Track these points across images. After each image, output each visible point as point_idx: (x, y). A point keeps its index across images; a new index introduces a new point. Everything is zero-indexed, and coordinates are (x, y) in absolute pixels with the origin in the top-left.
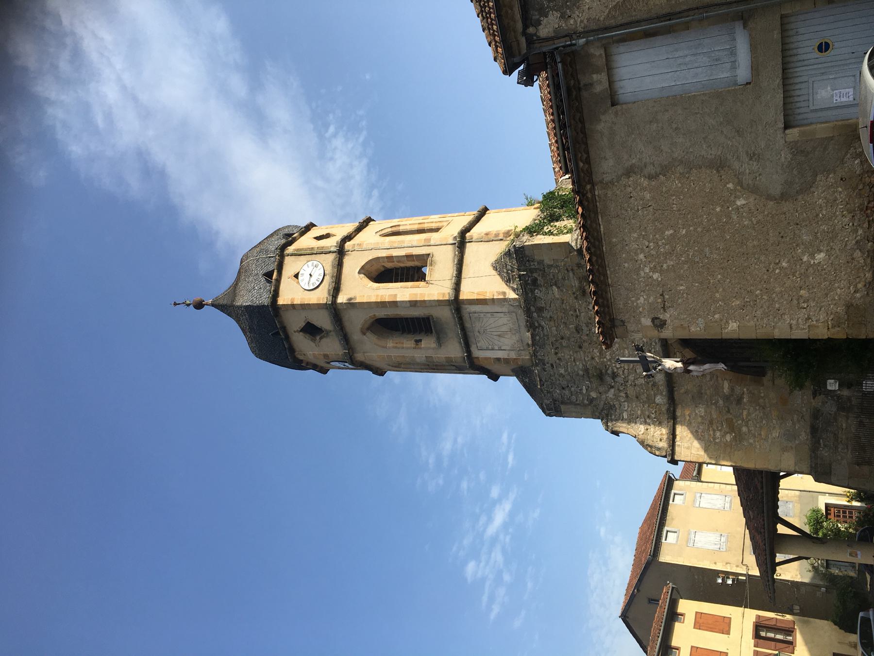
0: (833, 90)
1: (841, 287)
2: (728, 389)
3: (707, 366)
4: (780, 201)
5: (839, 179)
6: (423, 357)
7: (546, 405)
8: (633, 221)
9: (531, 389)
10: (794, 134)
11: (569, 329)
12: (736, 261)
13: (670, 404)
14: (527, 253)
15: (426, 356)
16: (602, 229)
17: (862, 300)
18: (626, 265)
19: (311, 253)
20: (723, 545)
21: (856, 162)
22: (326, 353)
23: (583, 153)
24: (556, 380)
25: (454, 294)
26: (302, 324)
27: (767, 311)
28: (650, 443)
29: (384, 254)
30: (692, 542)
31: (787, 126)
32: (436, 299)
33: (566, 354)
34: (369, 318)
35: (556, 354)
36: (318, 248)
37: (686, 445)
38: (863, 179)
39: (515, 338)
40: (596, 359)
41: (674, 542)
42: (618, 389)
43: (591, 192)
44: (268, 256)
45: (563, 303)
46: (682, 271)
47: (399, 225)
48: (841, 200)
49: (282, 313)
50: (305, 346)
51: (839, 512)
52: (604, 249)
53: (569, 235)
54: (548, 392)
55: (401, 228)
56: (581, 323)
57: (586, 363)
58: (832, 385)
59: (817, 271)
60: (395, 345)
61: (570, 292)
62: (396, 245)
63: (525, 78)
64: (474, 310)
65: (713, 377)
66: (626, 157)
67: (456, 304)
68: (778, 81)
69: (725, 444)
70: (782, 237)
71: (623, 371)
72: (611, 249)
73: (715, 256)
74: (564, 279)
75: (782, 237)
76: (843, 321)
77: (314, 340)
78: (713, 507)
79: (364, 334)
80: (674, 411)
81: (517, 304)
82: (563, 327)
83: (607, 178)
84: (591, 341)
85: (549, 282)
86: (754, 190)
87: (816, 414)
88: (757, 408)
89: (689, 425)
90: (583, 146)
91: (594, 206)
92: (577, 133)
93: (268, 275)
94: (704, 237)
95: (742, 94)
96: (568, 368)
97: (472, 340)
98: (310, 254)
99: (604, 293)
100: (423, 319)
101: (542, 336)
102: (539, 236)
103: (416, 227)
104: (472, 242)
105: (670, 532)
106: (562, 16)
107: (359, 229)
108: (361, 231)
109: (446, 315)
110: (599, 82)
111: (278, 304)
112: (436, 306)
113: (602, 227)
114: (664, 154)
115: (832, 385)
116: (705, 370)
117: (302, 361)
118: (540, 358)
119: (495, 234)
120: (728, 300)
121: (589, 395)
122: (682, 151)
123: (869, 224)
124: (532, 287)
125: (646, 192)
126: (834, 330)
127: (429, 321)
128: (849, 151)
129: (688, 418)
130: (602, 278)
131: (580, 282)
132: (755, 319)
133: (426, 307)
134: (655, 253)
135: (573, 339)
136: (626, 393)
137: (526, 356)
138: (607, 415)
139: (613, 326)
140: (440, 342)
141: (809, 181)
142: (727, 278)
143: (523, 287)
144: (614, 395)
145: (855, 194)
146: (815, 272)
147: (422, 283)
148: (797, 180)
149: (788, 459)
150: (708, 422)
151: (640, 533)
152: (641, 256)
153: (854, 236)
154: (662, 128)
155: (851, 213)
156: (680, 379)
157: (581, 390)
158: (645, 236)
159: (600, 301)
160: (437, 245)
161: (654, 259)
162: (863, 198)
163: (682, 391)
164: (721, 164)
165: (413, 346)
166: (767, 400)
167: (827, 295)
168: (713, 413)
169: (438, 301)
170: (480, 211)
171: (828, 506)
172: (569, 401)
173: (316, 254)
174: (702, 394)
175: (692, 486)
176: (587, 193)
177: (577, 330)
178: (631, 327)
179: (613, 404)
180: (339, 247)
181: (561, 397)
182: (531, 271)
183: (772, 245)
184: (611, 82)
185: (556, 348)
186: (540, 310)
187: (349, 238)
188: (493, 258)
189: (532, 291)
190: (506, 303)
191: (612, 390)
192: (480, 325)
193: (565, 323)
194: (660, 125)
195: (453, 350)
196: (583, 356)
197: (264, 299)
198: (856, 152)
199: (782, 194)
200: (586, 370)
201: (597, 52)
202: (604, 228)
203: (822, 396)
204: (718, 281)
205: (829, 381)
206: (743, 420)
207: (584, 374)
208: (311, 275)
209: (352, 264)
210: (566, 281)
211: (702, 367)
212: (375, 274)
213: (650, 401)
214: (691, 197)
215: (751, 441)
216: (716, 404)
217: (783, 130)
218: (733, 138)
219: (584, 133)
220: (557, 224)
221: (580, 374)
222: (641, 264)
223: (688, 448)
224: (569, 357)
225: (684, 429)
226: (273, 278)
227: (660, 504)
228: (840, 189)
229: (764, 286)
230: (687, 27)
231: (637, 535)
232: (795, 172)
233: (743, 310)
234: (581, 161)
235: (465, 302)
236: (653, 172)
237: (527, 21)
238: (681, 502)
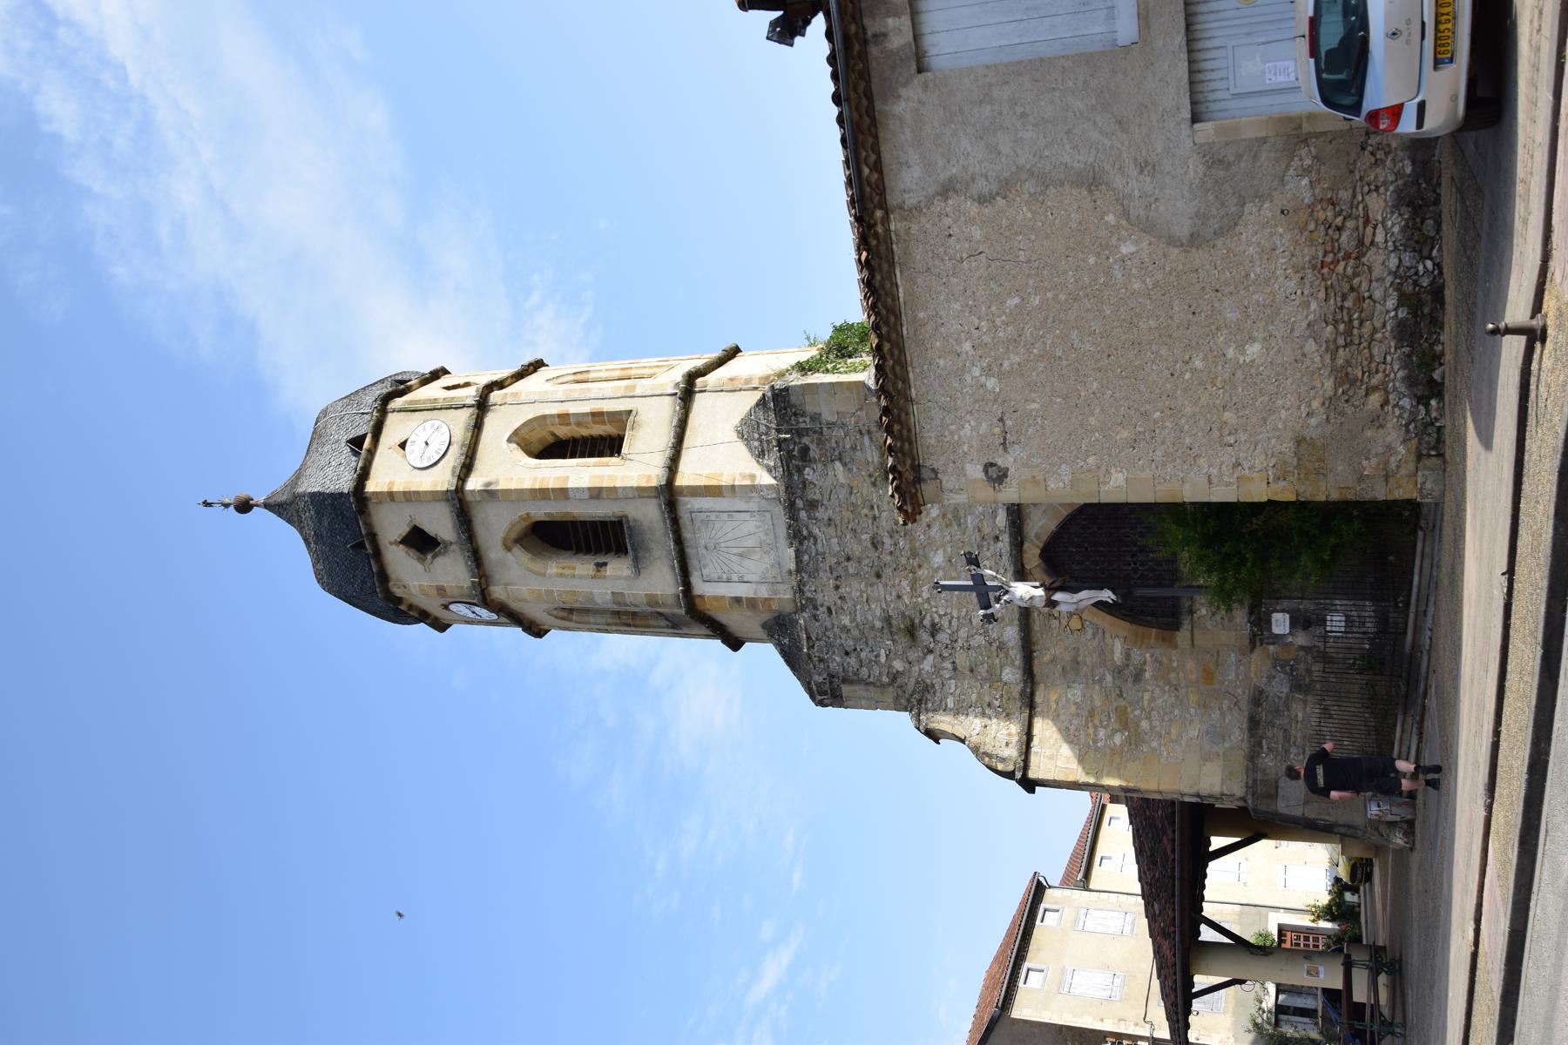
0: (1264, 62)
1: (1287, 407)
2: (1121, 654)
3: (1084, 594)
4: (1188, 248)
5: (1279, 211)
6: (607, 593)
7: (816, 685)
8: (954, 280)
9: (792, 658)
10: (1206, 130)
11: (860, 541)
12: (1122, 356)
13: (1025, 682)
14: (793, 399)
15: (613, 593)
16: (901, 295)
17: (1320, 429)
18: (942, 362)
19: (433, 408)
20: (1116, 992)
21: (1303, 183)
22: (441, 584)
23: (870, 152)
24: (835, 639)
25: (666, 475)
26: (404, 530)
27: (1171, 449)
28: (988, 748)
30: (1067, 986)
31: (1195, 118)
32: (635, 485)
33: (853, 589)
34: (518, 519)
35: (837, 588)
36: (444, 399)
37: (1048, 752)
38: (1315, 213)
39: (768, 560)
40: (905, 597)
41: (1039, 987)
42: (941, 655)
43: (883, 225)
44: (361, 411)
45: (851, 493)
46: (1034, 374)
48: (1282, 250)
49: (372, 508)
50: (410, 575)
51: (1298, 938)
52: (905, 332)
54: (821, 660)
56: (880, 532)
57: (888, 605)
58: (1280, 623)
59: (1249, 377)
60: (560, 571)
61: (863, 473)
62: (576, 396)
63: (778, 29)
64: (700, 506)
65: (1098, 632)
66: (941, 162)
68: (1180, 39)
69: (1112, 750)
70: (1194, 313)
71: (950, 622)
72: (915, 331)
73: (1088, 346)
74: (854, 448)
75: (1194, 313)
76: (1292, 469)
77: (422, 561)
78: (1106, 931)
79: (509, 549)
80: (1032, 694)
81: (774, 495)
82: (852, 538)
83: (911, 200)
84: (898, 565)
85: (829, 454)
86: (1147, 227)
87: (1258, 698)
88: (1167, 688)
89: (1056, 719)
90: (871, 140)
91: (887, 249)
92: (861, 116)
93: (357, 443)
94: (1070, 311)
95: (1125, 58)
96: (856, 616)
97: (693, 563)
98: (431, 410)
99: (903, 414)
100: (613, 523)
101: (813, 554)
102: (816, 375)
103: (617, 374)
104: (705, 391)
105: (1033, 970)
107: (520, 375)
108: (523, 378)
109: (650, 515)
110: (897, 31)
111: (366, 490)
112: (634, 498)
113: (901, 290)
114: (1003, 160)
115: (1280, 623)
116: (1081, 600)
117: (400, 600)
118: (809, 595)
119: (745, 379)
120: (1109, 429)
121: (890, 667)
122: (1032, 154)
123: (1327, 294)
124: (800, 464)
125: (974, 227)
126: (1277, 486)
127: (622, 524)
128: (1292, 163)
129: (1054, 706)
130: (900, 384)
132: (1153, 466)
133: (617, 499)
134: (990, 341)
135: (867, 561)
136: (954, 663)
137: (786, 594)
138: (920, 702)
139: (918, 480)
141: (1232, 213)
142: (1108, 388)
143: (784, 462)
145: (1304, 240)
146: (1245, 378)
148: (1214, 212)
150: (1087, 713)
152: (967, 346)
153: (1305, 313)
154: (1000, 113)
155: (1298, 272)
156: (1044, 636)
157: (876, 656)
158: (974, 309)
159: (896, 428)
160: (645, 396)
161: (988, 351)
162: (1316, 246)
163: (1047, 658)
164: (1094, 178)
165: (592, 573)
166: (1181, 673)
167: (1265, 420)
168: (1095, 698)
170: (726, 351)
171: (1282, 930)
172: (855, 678)
173: (441, 409)
174: (1078, 663)
175: (1073, 897)
176: (875, 224)
177: (873, 543)
178: (948, 481)
179: (932, 683)
180: (481, 397)
181: (844, 669)
182: (800, 433)
183: (1178, 327)
184: (917, 36)
185: (838, 578)
186: (812, 505)
187: (500, 385)
188: (736, 420)
189: (800, 471)
190: (754, 494)
191: (930, 657)
192: (709, 534)
193: (854, 531)
194: (996, 107)
195: (660, 582)
196: (882, 592)
197: (345, 483)
198: (1302, 165)
199: (1192, 235)
200: (888, 620)
202: (904, 293)
204: (1094, 393)
206: (1143, 709)
207: (883, 627)
208: (427, 444)
209: (499, 425)
210: (859, 453)
211: (1075, 595)
212: (537, 448)
213: (993, 677)
214: (1047, 237)
215: (1154, 744)
217: (1189, 124)
218: (1113, 134)
219: (871, 111)
221: (876, 627)
222: (966, 361)
223: (1051, 758)
224: (858, 594)
225: (1047, 724)
226: (363, 447)
227: (1020, 925)
228: (1281, 230)
229: (1167, 403)
232: (1211, 198)
233: (1134, 448)
234: (867, 165)
235: (685, 492)
236: (986, 191)
238: (1055, 922)
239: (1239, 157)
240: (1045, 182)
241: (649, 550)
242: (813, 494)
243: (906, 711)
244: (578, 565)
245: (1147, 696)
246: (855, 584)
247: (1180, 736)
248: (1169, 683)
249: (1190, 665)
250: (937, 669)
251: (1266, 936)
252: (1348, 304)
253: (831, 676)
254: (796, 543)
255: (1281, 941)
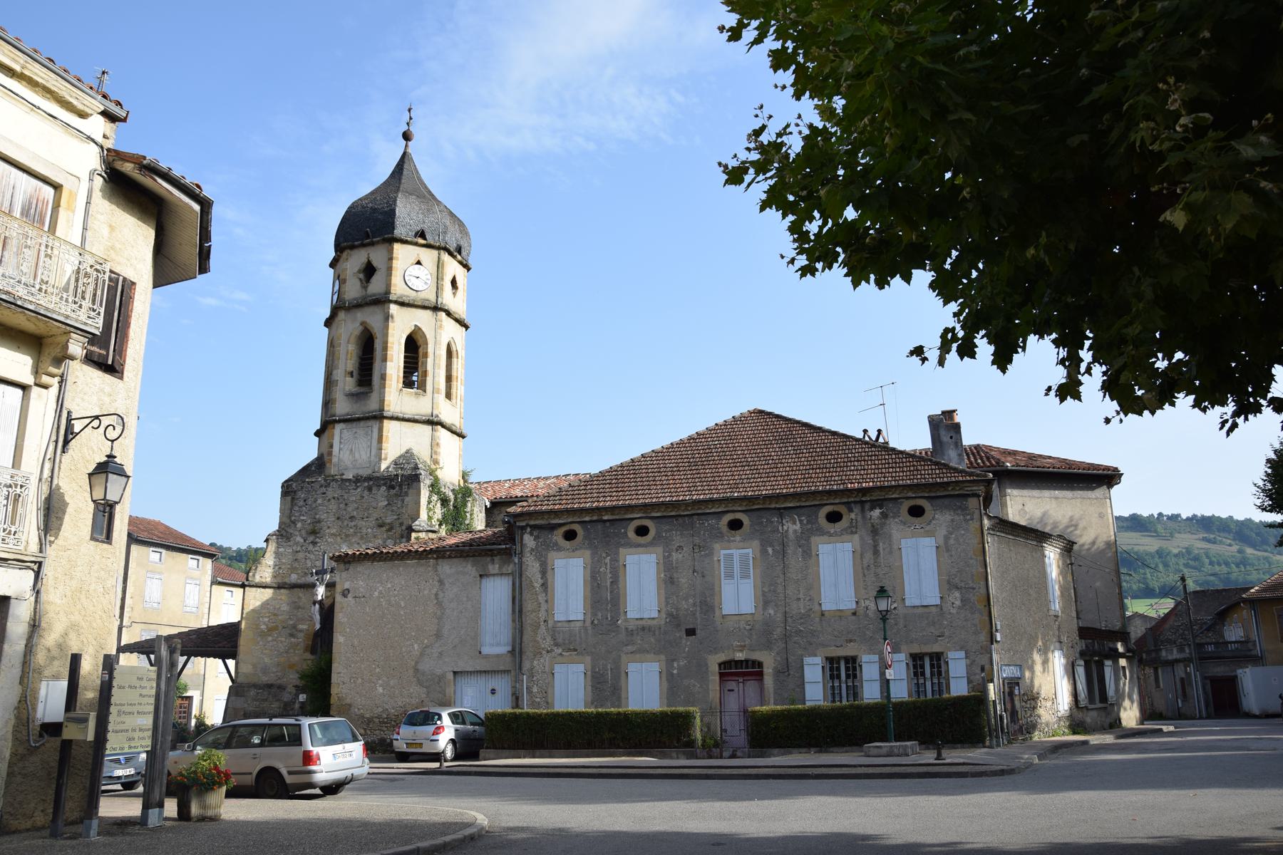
9: (305, 471)
10: (451, 676)
11: (353, 511)
19: (439, 278)
26: (375, 264)
29: (430, 350)
30: (152, 576)
31: (455, 673)
33: (333, 506)
35: (334, 498)
39: (348, 463)
47: (457, 358)
49: (387, 245)
50: (356, 260)
51: (185, 708)
53: (426, 517)
54: (302, 488)
55: (454, 360)
58: (302, 697)
67: (379, 417)
68: (478, 669)
77: (359, 272)
80: (284, 588)
83: (439, 568)
86: (422, 654)
87: (281, 688)
89: (272, 599)
97: (349, 425)
103: (454, 374)
106: (532, 550)
115: (302, 697)
121: (299, 521)
131: (389, 524)
137: (333, 471)
138: (282, 535)
139: (345, 563)
140: (351, 395)
144: (298, 542)
147: (401, 385)
149: (247, 669)
151: (154, 521)
152: (389, 586)
163: (301, 595)
165: (348, 369)
169: (384, 400)
171: (190, 698)
178: (344, 574)
182: (401, 486)
184: (494, 575)
186: (370, 489)
189: (385, 484)
191: (302, 541)
193: (358, 508)
195: (342, 407)
197: (399, 231)
200: (319, 521)
201: (510, 568)
203: (294, 692)
205: (305, 696)
206: (277, 637)
209: (423, 319)
212: (413, 335)
213: (293, 569)
215: (261, 643)
216: (290, 618)
219: (467, 556)
220: (439, 505)
230: (514, 621)
231: (152, 518)
237: (534, 527)
239: (441, 687)
240: (440, 619)
241: (356, 402)
242: (374, 490)
243: (279, 527)
244: (352, 362)
245: (283, 639)
246: (335, 507)
247: (265, 654)
248: (289, 649)
249: (296, 658)
250: (297, 543)
251: (185, 688)
252: (393, 723)
253: (295, 492)
254: (354, 479)
255: (183, 698)
